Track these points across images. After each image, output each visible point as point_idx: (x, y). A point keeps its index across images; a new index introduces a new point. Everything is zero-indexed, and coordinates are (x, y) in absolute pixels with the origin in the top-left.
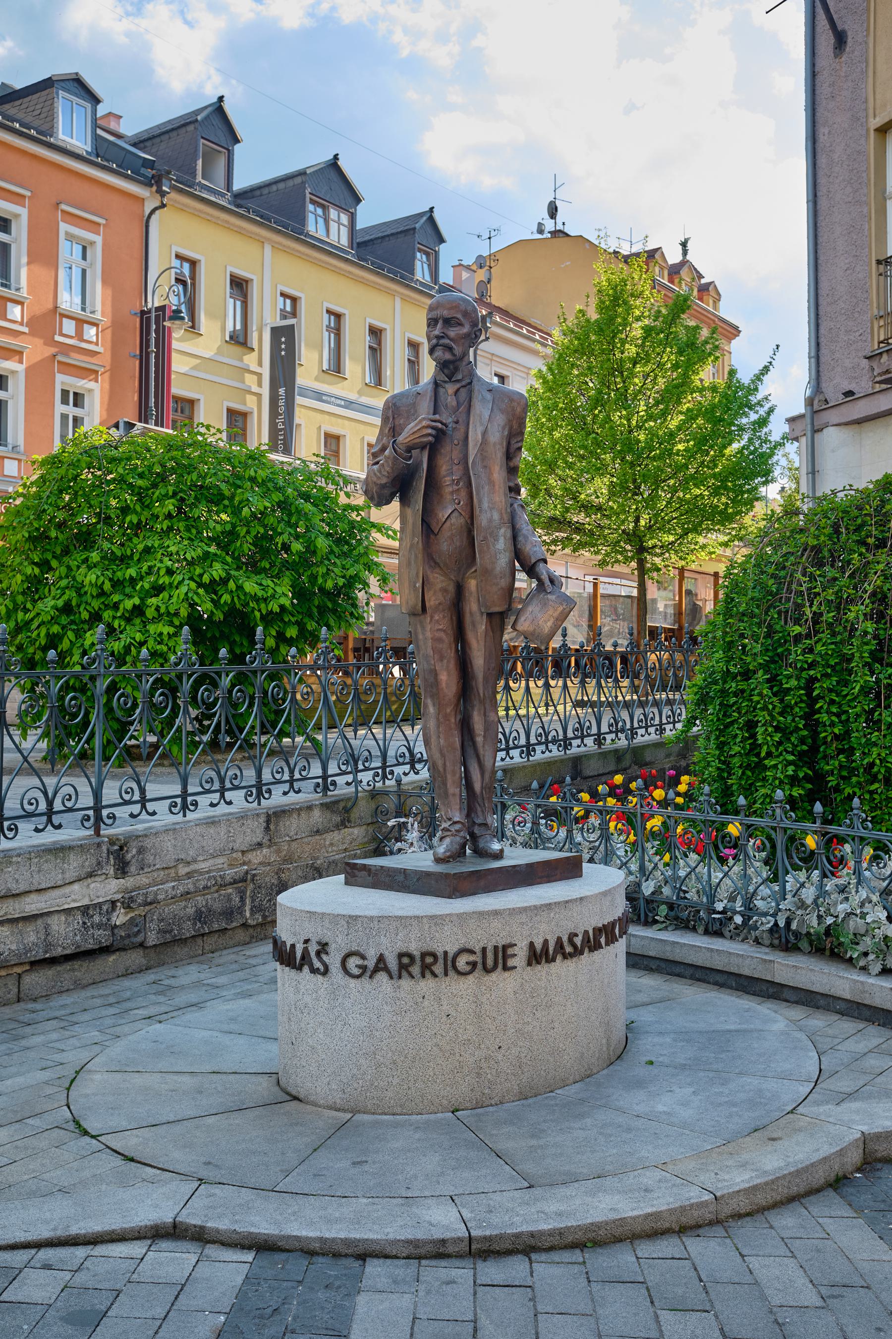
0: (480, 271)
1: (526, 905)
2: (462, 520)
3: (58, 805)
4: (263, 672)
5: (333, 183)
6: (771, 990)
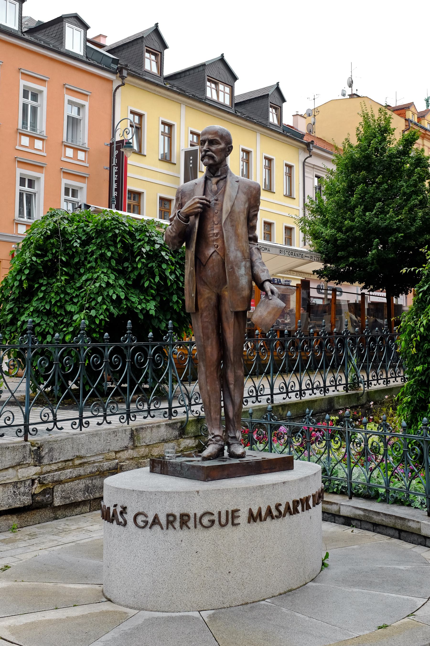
2: (219, 257)
5: (222, 70)
6: (420, 540)
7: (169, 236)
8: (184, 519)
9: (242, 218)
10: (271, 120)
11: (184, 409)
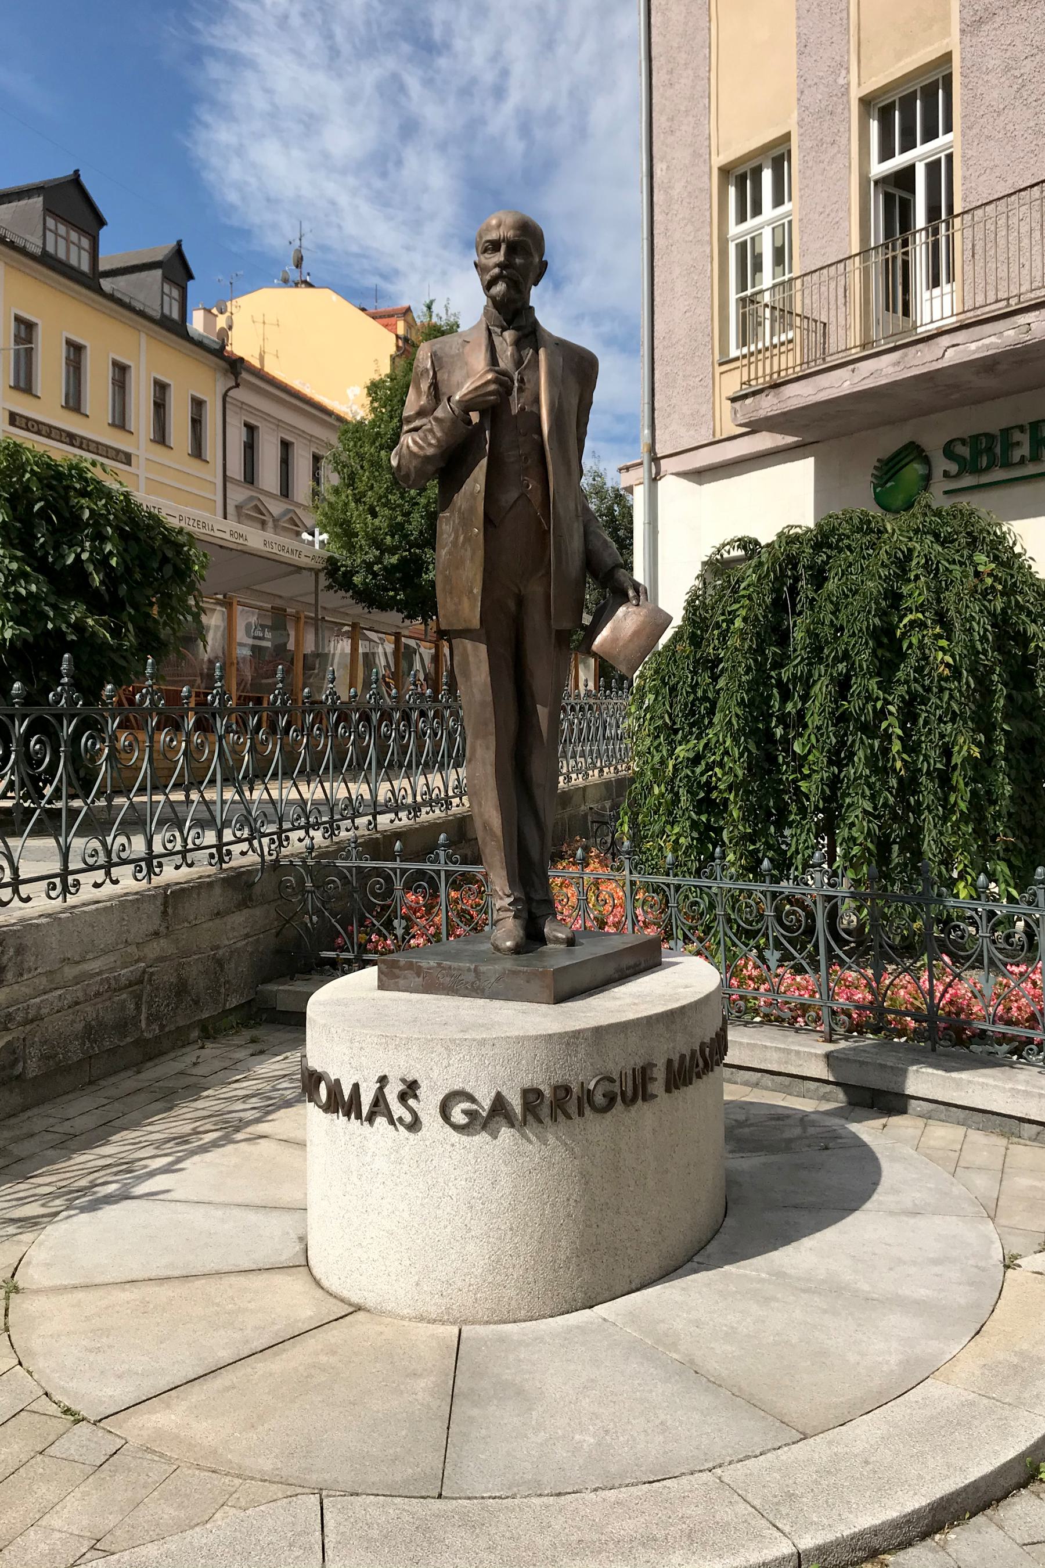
0: (220, 316)
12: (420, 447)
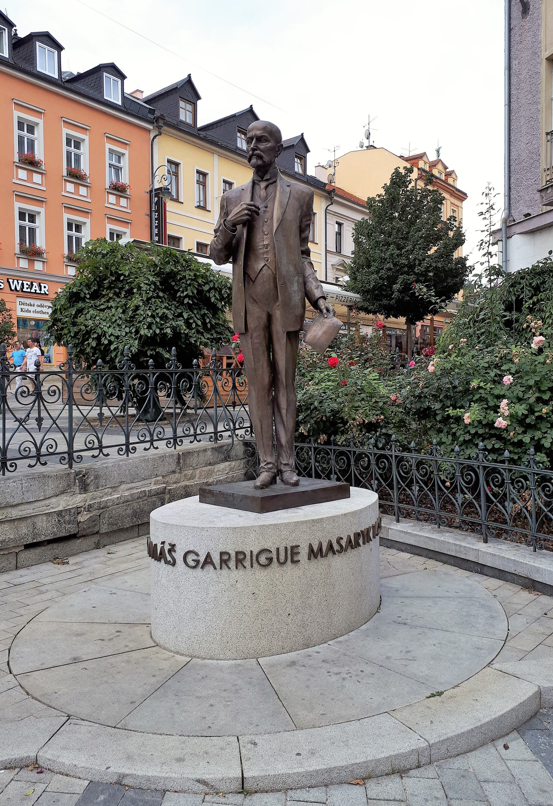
1: (306, 519)
3: (43, 450)
4: (176, 373)
6: (476, 568)
7: (214, 248)
8: (240, 558)
9: (295, 228)
10: (296, 170)
11: (229, 433)
12: (217, 245)
